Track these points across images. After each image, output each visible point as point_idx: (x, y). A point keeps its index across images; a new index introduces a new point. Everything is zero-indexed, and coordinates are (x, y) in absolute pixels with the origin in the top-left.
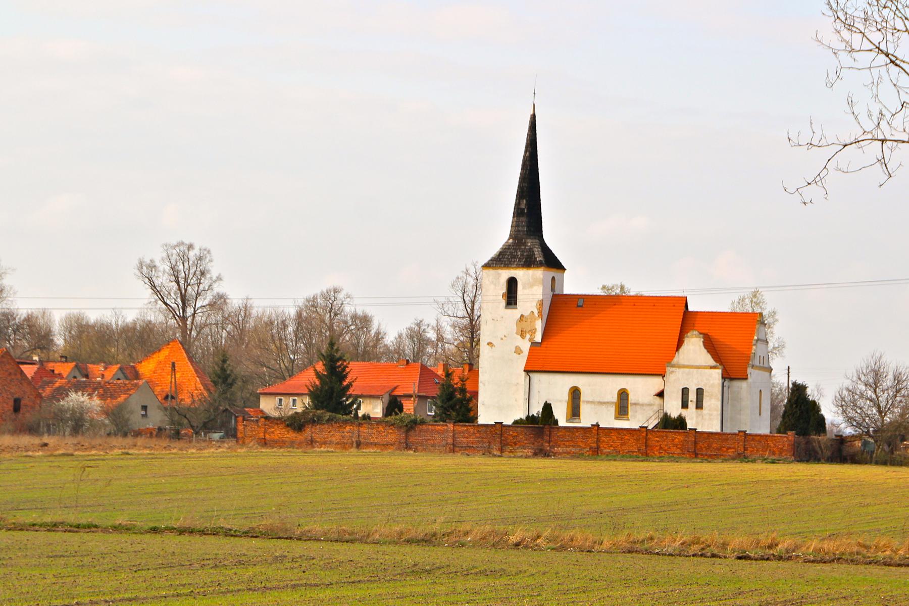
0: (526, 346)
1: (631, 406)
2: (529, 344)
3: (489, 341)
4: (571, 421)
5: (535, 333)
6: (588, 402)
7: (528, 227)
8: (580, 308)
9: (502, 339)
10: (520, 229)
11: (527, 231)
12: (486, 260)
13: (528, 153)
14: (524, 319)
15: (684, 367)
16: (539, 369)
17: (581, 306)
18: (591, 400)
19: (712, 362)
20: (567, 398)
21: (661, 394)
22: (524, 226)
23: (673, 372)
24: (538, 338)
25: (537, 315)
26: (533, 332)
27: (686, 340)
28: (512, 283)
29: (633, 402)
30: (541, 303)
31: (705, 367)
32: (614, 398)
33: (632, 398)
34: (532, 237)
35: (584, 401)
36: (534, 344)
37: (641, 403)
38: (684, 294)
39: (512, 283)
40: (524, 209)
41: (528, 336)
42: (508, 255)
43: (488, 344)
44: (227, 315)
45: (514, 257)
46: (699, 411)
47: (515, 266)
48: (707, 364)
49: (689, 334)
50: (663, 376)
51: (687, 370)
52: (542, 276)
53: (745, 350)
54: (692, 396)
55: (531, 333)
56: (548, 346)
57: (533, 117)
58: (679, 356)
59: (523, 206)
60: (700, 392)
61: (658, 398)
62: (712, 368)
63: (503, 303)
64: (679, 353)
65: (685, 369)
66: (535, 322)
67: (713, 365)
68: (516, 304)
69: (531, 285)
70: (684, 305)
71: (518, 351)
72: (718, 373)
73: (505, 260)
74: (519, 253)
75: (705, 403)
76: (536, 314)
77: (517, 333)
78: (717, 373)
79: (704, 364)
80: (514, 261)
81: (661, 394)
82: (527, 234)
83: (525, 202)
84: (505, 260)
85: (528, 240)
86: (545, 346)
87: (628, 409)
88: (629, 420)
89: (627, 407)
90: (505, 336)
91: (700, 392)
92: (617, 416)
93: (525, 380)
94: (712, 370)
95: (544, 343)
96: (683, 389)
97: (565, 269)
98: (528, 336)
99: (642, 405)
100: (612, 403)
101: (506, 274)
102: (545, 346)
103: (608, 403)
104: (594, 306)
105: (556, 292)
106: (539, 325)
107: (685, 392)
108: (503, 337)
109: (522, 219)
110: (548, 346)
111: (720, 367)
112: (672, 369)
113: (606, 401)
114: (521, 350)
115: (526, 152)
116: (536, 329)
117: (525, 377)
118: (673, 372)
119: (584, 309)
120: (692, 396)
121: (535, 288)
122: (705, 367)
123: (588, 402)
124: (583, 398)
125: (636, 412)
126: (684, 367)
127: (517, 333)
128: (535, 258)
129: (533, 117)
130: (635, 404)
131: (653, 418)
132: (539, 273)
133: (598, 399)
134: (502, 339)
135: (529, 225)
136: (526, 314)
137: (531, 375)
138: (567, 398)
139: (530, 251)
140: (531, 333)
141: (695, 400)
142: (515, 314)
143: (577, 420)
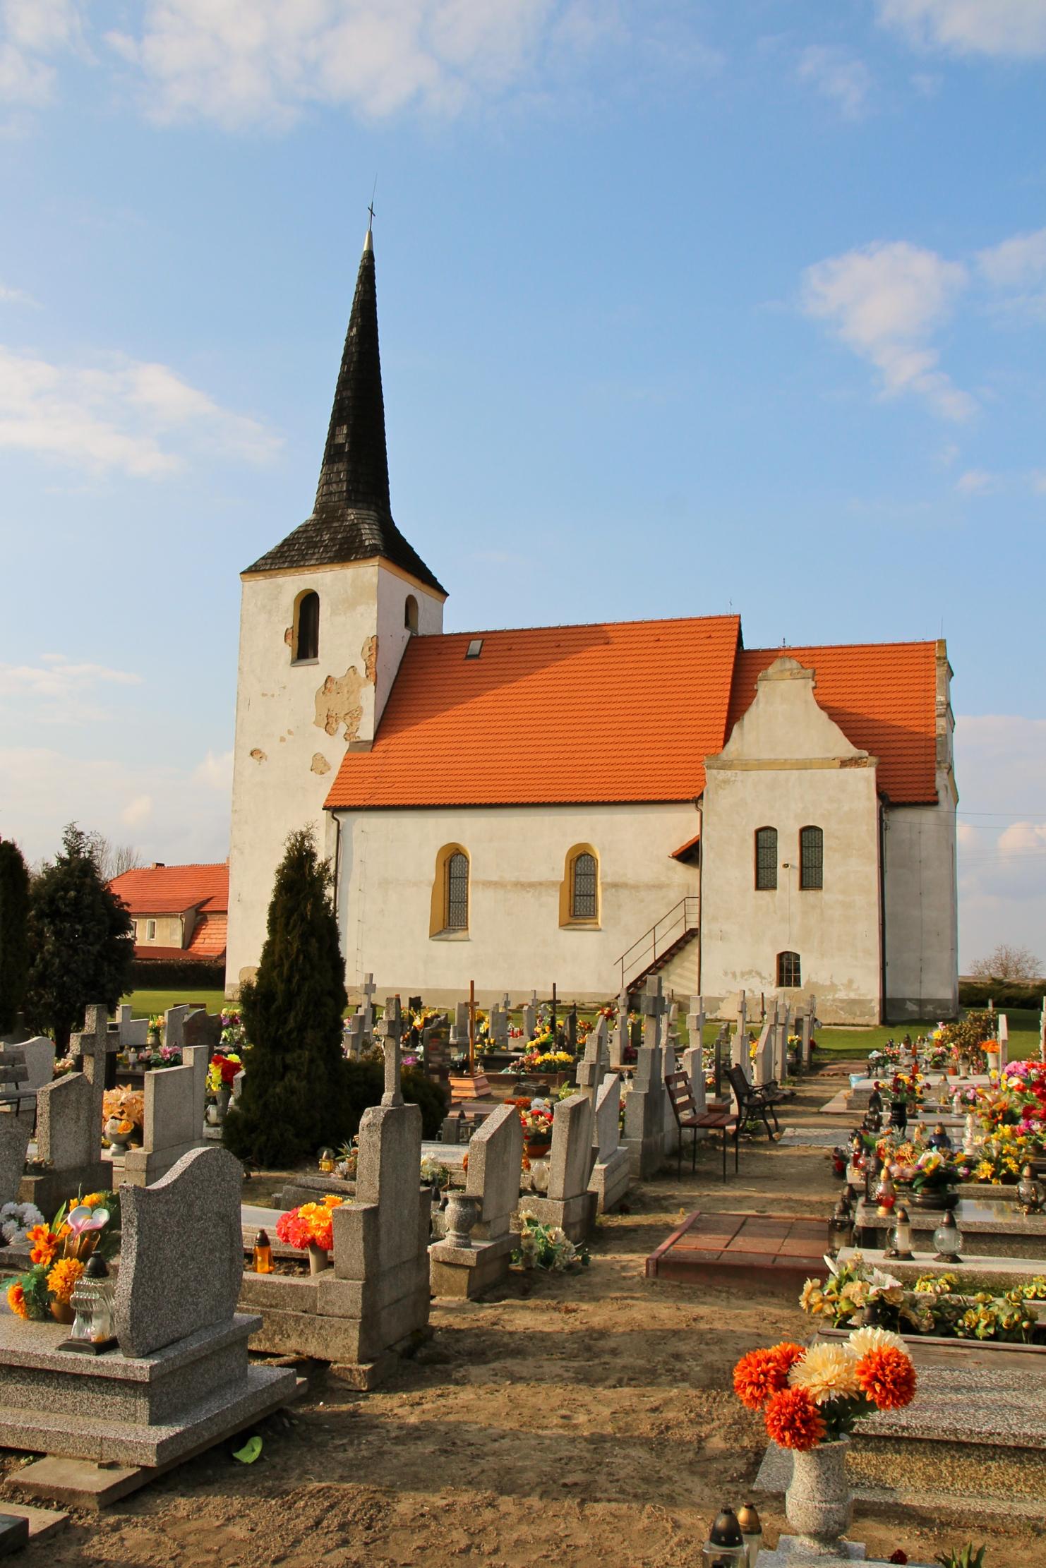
0: (336, 750)
1: (604, 890)
2: (346, 746)
3: (249, 752)
4: (444, 936)
5: (358, 718)
6: (488, 884)
7: (349, 482)
8: (473, 661)
9: (283, 739)
10: (334, 488)
11: (347, 491)
12: (245, 568)
13: (354, 330)
14: (334, 687)
15: (761, 765)
16: (361, 803)
17: (476, 656)
18: (495, 878)
19: (849, 750)
20: (432, 876)
21: (690, 855)
22: (341, 481)
23: (726, 782)
24: (367, 731)
25: (364, 676)
26: (354, 715)
27: (763, 688)
28: (308, 605)
29: (609, 880)
30: (376, 645)
31: (824, 764)
32: (559, 871)
33: (605, 871)
34: (360, 505)
35: (476, 883)
36: (357, 746)
37: (631, 882)
38: (734, 611)
39: (308, 605)
40: (343, 445)
41: (343, 728)
42: (303, 543)
43: (252, 754)
44: (995, 1153)
45: (315, 545)
46: (811, 895)
47: (313, 562)
48: (832, 755)
49: (771, 670)
50: (697, 800)
51: (767, 775)
52: (375, 580)
53: (911, 723)
54: (788, 852)
55: (348, 721)
56: (391, 748)
57: (370, 256)
58: (742, 734)
59: (340, 440)
60: (810, 838)
61: (680, 867)
62: (844, 764)
63: (286, 651)
64: (741, 727)
65: (762, 773)
66: (359, 691)
67: (850, 755)
68: (316, 655)
69: (351, 604)
70: (735, 640)
71: (319, 765)
72: (867, 780)
73: (293, 553)
74: (326, 537)
75: (831, 869)
76: (362, 672)
77: (317, 723)
78: (864, 780)
79: (818, 754)
80: (314, 554)
81: (690, 855)
82: (349, 499)
83: (345, 431)
84: (293, 553)
85: (350, 511)
86: (382, 748)
87: (595, 901)
88: (600, 930)
89: (594, 895)
90: (290, 732)
91: (810, 838)
92: (567, 918)
93: (327, 832)
94: (847, 771)
95: (383, 742)
96: (758, 832)
97: (447, 595)
98: (343, 728)
99: (636, 887)
100: (553, 884)
101: (292, 584)
102: (382, 748)
103: (541, 884)
104: (508, 653)
105: (424, 629)
106: (368, 702)
107: (765, 840)
108: (288, 737)
109: (341, 466)
110: (391, 748)
111: (873, 760)
112: (723, 774)
113: (534, 879)
114: (326, 764)
115: (350, 328)
116: (360, 709)
117: (328, 826)
118: (726, 782)
119: (483, 661)
120: (788, 852)
121: (361, 609)
122: (824, 764)
123: (488, 884)
124: (475, 873)
125: (619, 906)
126: (761, 765)
127: (317, 723)
128: (362, 541)
129: (370, 256)
130: (615, 886)
131: (667, 922)
132: (369, 572)
133: (510, 876)
134: (283, 739)
135: (353, 478)
136: (337, 675)
137: (343, 818)
138: (434, 876)
139: (351, 530)
140: (348, 721)
141: (796, 863)
142: (313, 674)
143: (460, 935)
